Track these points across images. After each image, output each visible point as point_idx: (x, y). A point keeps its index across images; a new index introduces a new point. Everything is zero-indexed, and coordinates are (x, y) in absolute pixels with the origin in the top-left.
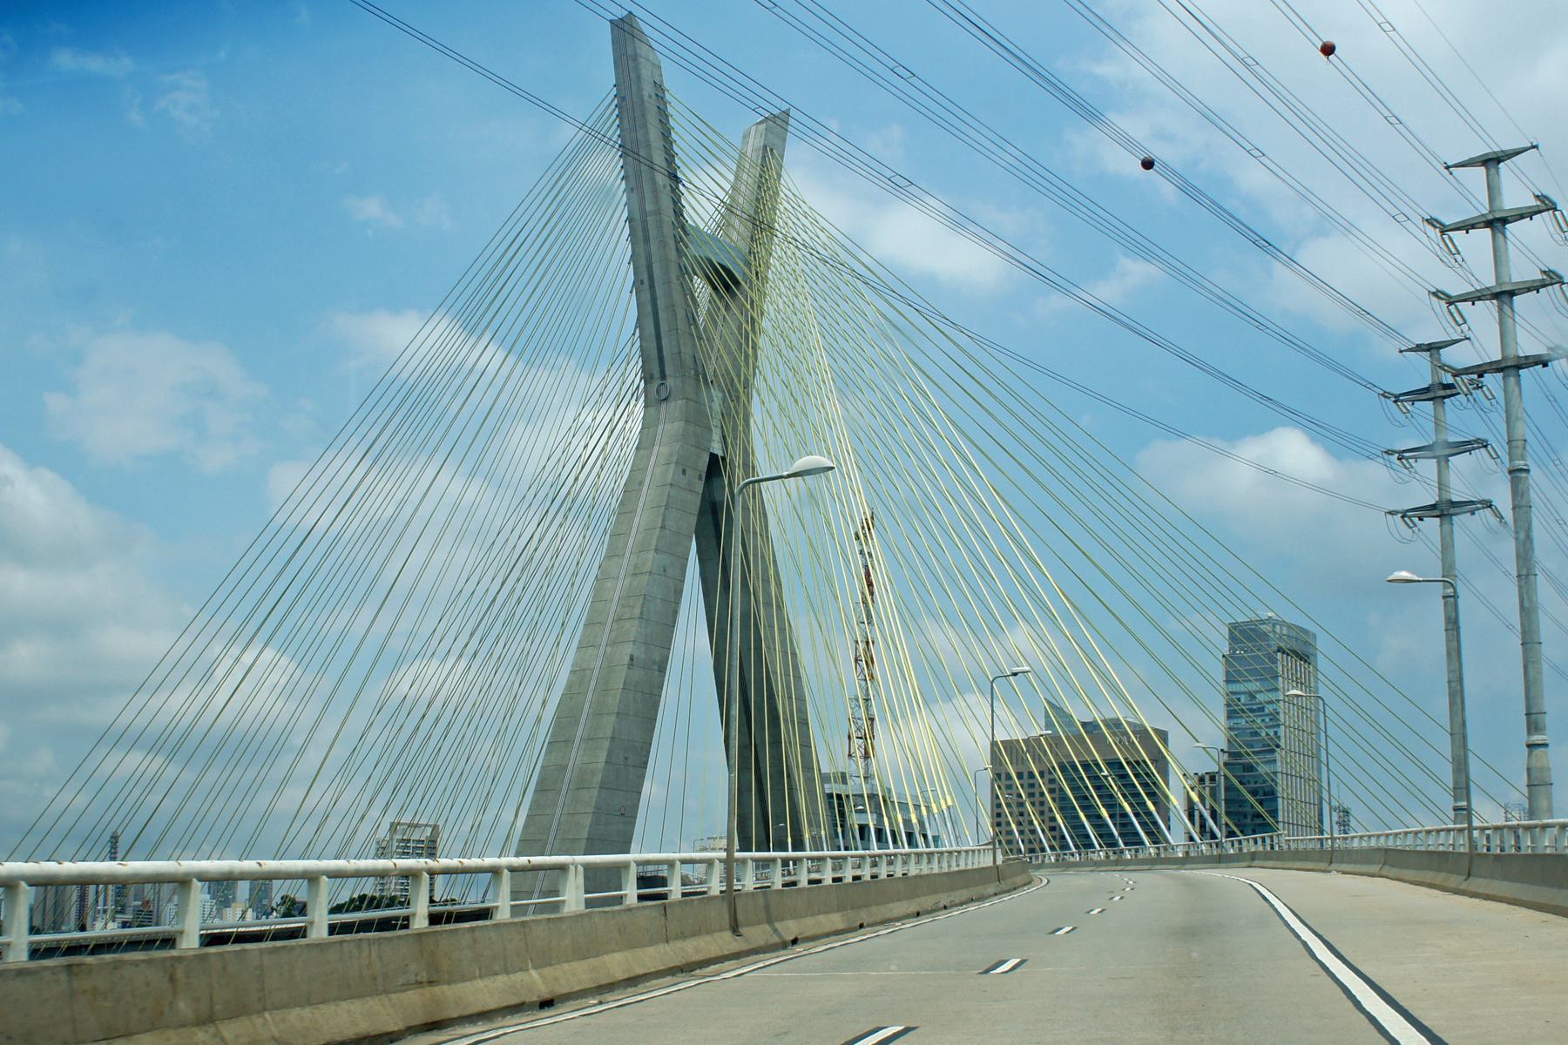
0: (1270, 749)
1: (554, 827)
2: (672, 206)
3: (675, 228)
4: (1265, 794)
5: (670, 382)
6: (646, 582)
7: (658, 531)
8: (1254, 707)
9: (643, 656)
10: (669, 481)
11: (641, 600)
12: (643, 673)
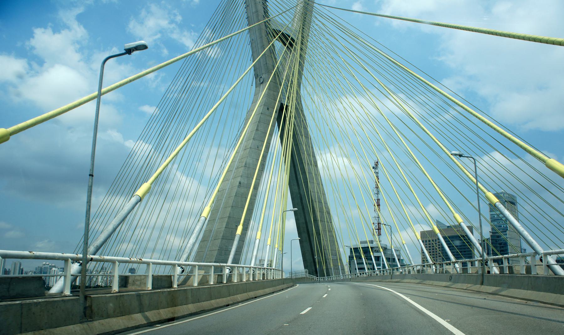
0: (505, 230)
4: (504, 244)
8: (499, 219)
9: (246, 182)
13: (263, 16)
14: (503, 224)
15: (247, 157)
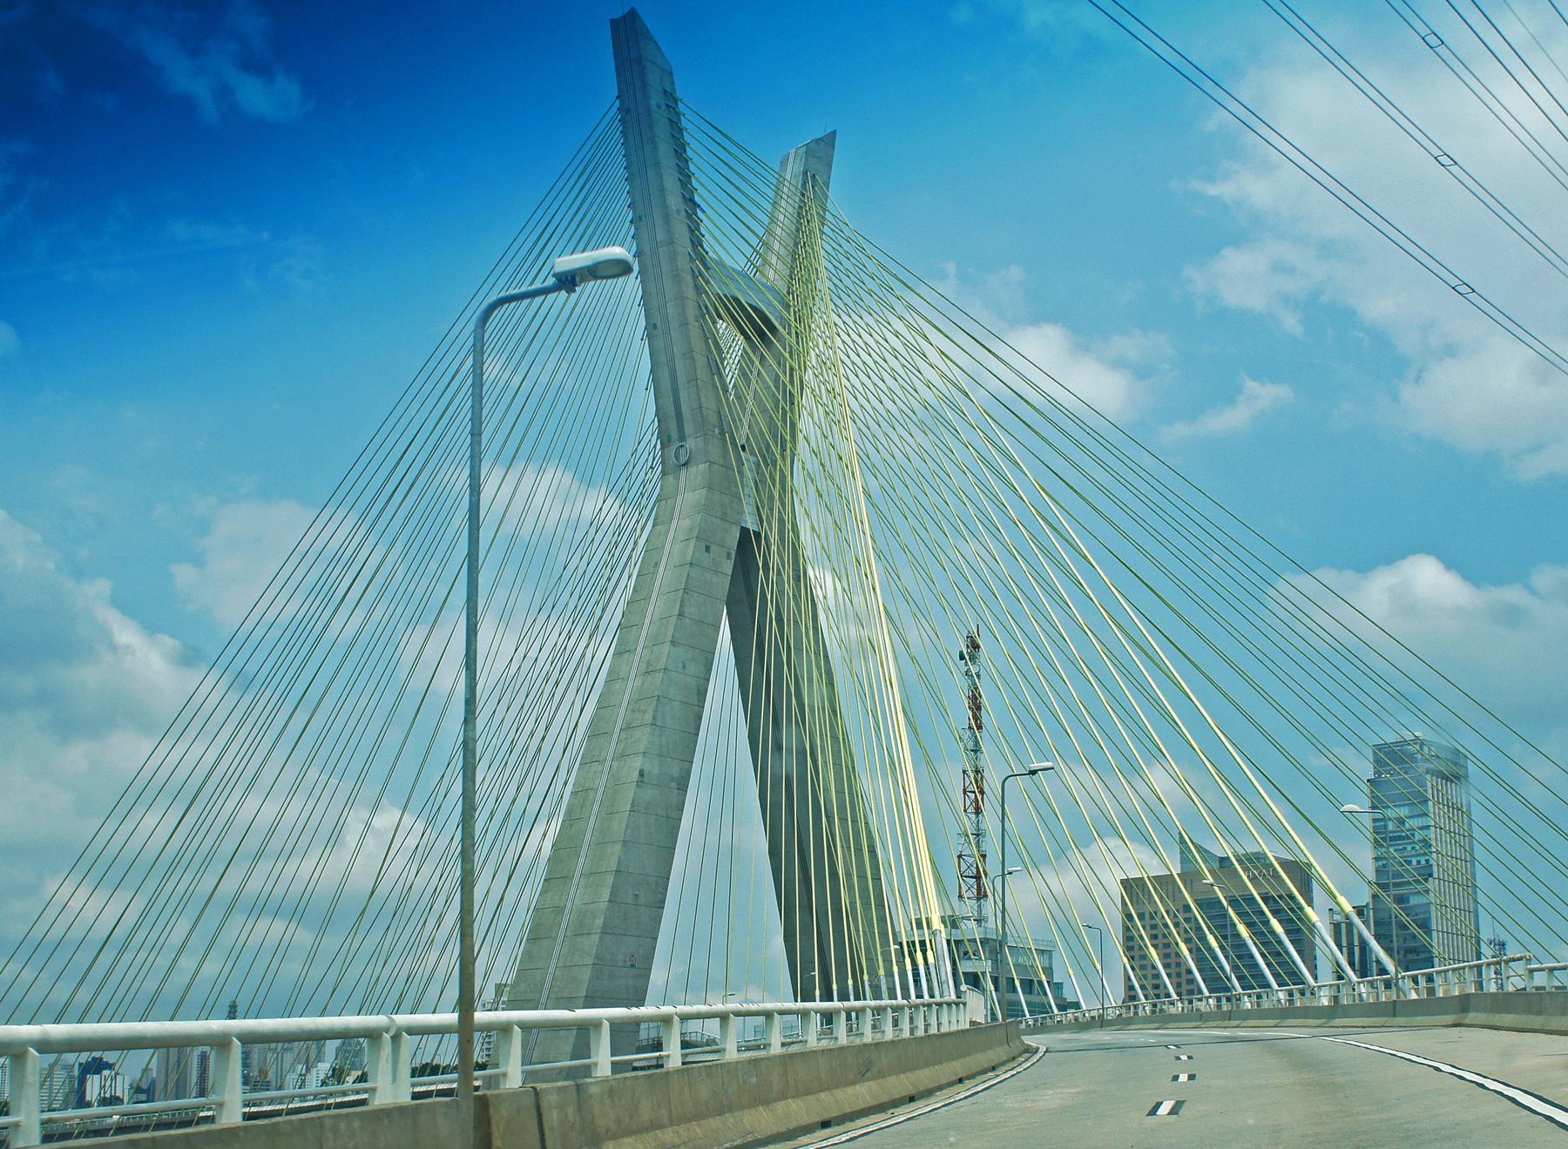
1: (547, 985)
2: (688, 235)
3: (692, 261)
5: (690, 444)
6: (659, 681)
7: (674, 619)
9: (656, 771)
10: (688, 559)
11: (655, 702)
12: (658, 792)
13: (689, 254)
14: (1418, 855)
15: (658, 696)
